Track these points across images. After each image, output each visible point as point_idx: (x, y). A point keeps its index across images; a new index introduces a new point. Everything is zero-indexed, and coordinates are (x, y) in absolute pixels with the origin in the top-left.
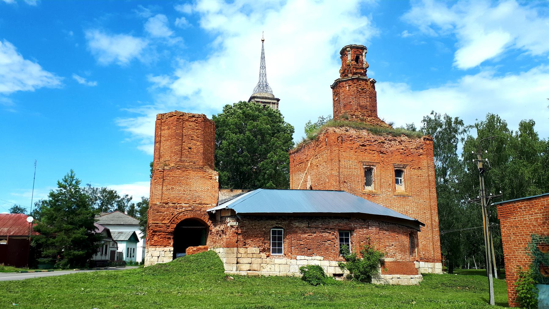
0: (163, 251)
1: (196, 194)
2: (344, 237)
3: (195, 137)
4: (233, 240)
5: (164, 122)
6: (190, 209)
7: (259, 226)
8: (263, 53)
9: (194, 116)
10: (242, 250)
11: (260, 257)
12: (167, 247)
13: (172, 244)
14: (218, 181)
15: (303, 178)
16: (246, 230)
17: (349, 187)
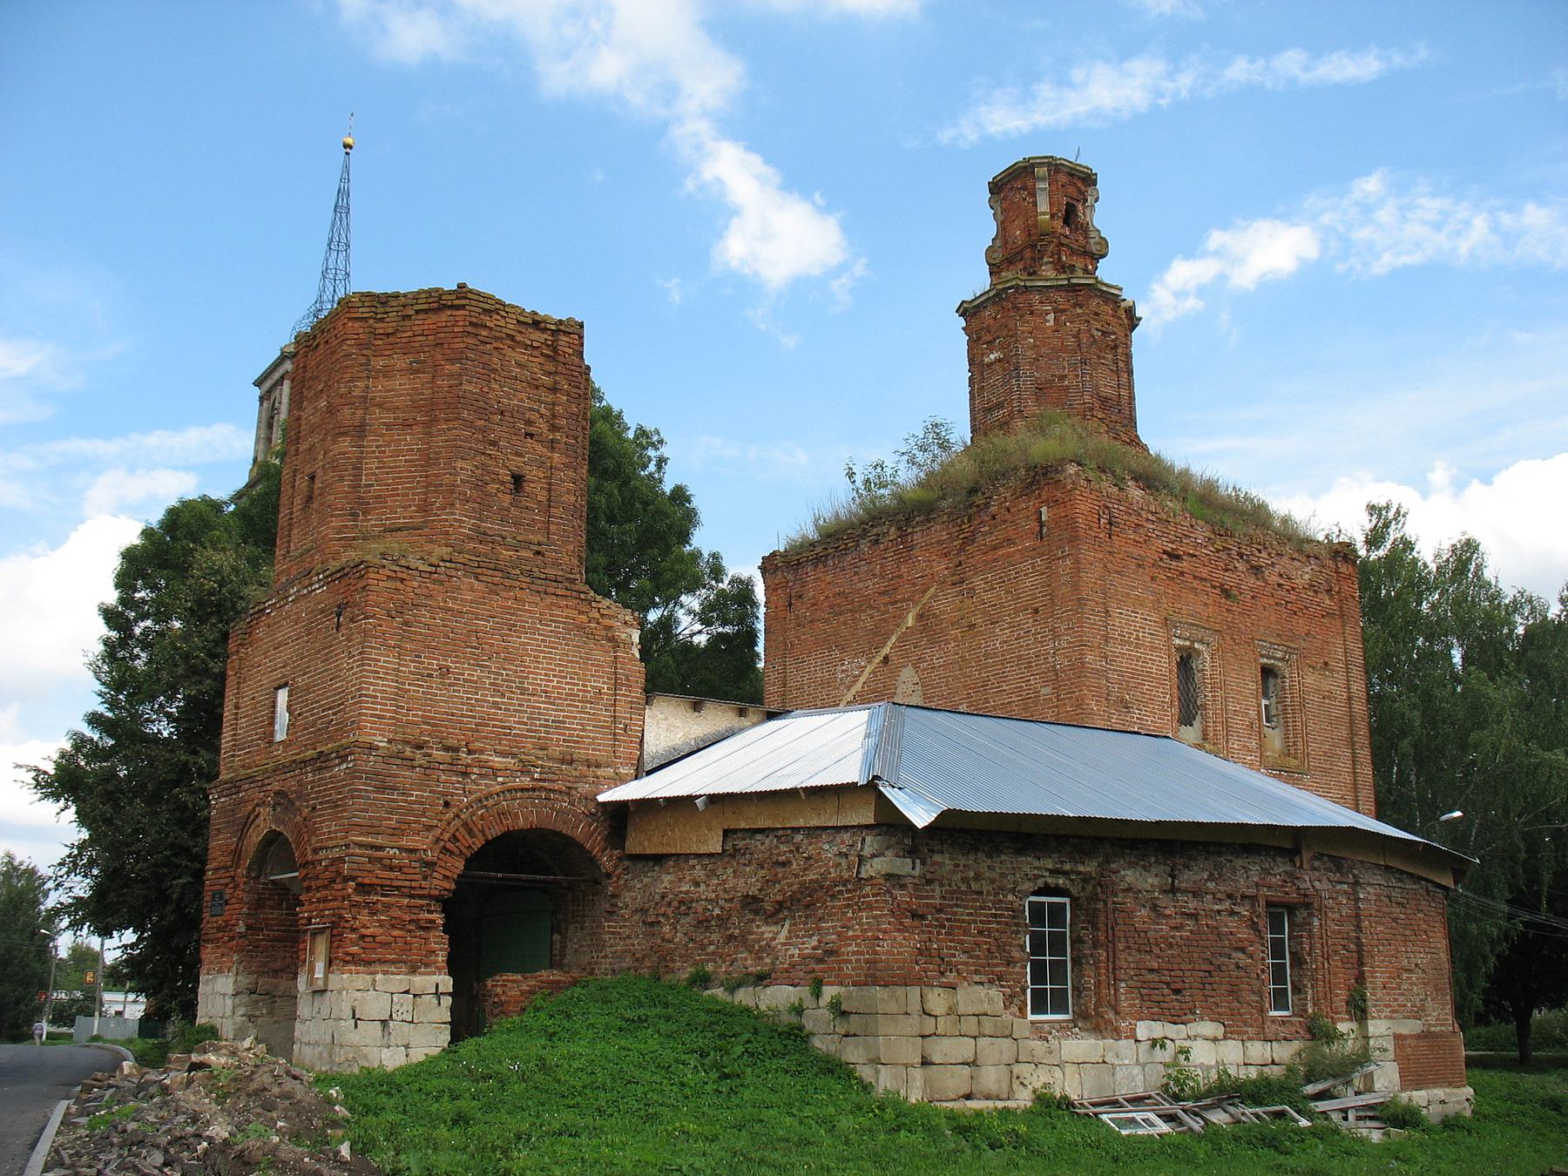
0: (407, 992)
1: (548, 709)
3: (542, 426)
4: (901, 946)
5: (388, 335)
6: (526, 781)
7: (992, 881)
8: (343, 193)
9: (539, 322)
10: (937, 1000)
11: (1007, 1032)
12: (420, 974)
13: (441, 958)
14: (638, 655)
15: (862, 680)
16: (945, 898)
17: (1135, 723)
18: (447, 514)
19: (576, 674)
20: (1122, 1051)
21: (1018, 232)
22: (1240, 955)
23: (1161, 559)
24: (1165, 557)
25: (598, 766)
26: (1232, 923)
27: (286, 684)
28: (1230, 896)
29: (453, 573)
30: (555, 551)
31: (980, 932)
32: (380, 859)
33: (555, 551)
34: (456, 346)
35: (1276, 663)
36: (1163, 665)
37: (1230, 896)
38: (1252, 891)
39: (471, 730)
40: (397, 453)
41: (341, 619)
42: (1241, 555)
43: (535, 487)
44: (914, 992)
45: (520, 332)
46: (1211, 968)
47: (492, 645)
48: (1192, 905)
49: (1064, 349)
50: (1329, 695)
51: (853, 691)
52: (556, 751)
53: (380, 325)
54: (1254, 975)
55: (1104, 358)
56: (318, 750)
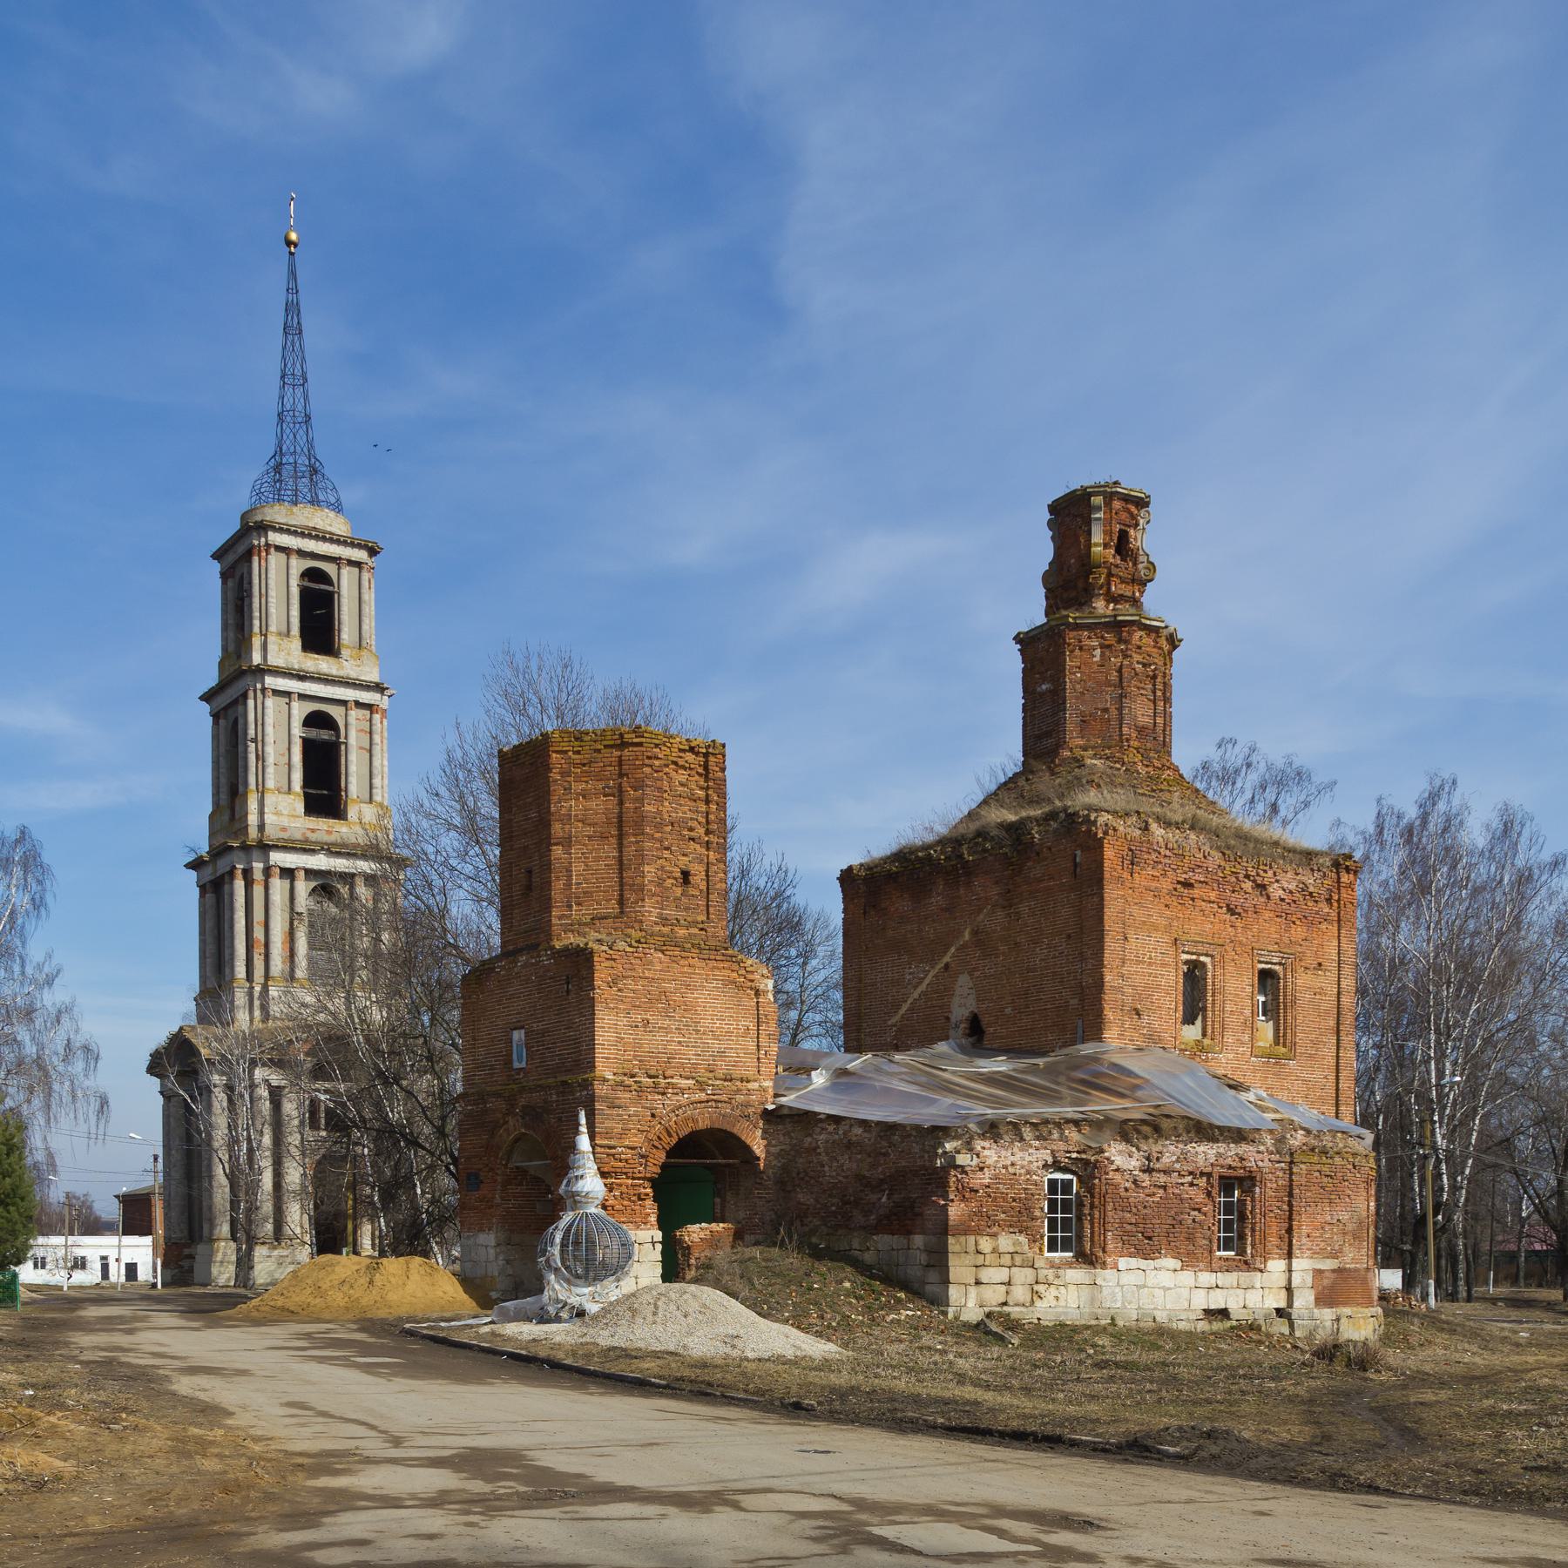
2: (1059, 1197)
6: (703, 1096)
10: (986, 1244)
13: (653, 1218)
15: (927, 981)
18: (640, 907)
19: (731, 1017)
20: (1107, 1277)
21: (1073, 561)
22: (1196, 1213)
23: (1175, 889)
24: (1179, 886)
25: (748, 1081)
26: (1192, 1191)
27: (522, 1027)
28: (1191, 1173)
29: (648, 951)
30: (713, 927)
31: (1014, 1200)
32: (613, 1155)
33: (713, 927)
34: (637, 776)
35: (1273, 967)
36: (1171, 981)
37: (1191, 1173)
38: (1209, 1170)
39: (665, 1062)
40: (597, 859)
41: (570, 986)
42: (1247, 876)
43: (698, 879)
44: (972, 1239)
45: (681, 757)
46: (1174, 1222)
47: (675, 1001)
48: (1162, 1179)
49: (1108, 683)
50: (1320, 992)
51: (919, 990)
52: (720, 1073)
53: (577, 756)
54: (1206, 1227)
55: (1143, 689)
56: (559, 1079)
